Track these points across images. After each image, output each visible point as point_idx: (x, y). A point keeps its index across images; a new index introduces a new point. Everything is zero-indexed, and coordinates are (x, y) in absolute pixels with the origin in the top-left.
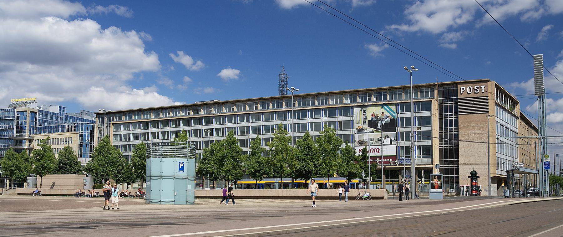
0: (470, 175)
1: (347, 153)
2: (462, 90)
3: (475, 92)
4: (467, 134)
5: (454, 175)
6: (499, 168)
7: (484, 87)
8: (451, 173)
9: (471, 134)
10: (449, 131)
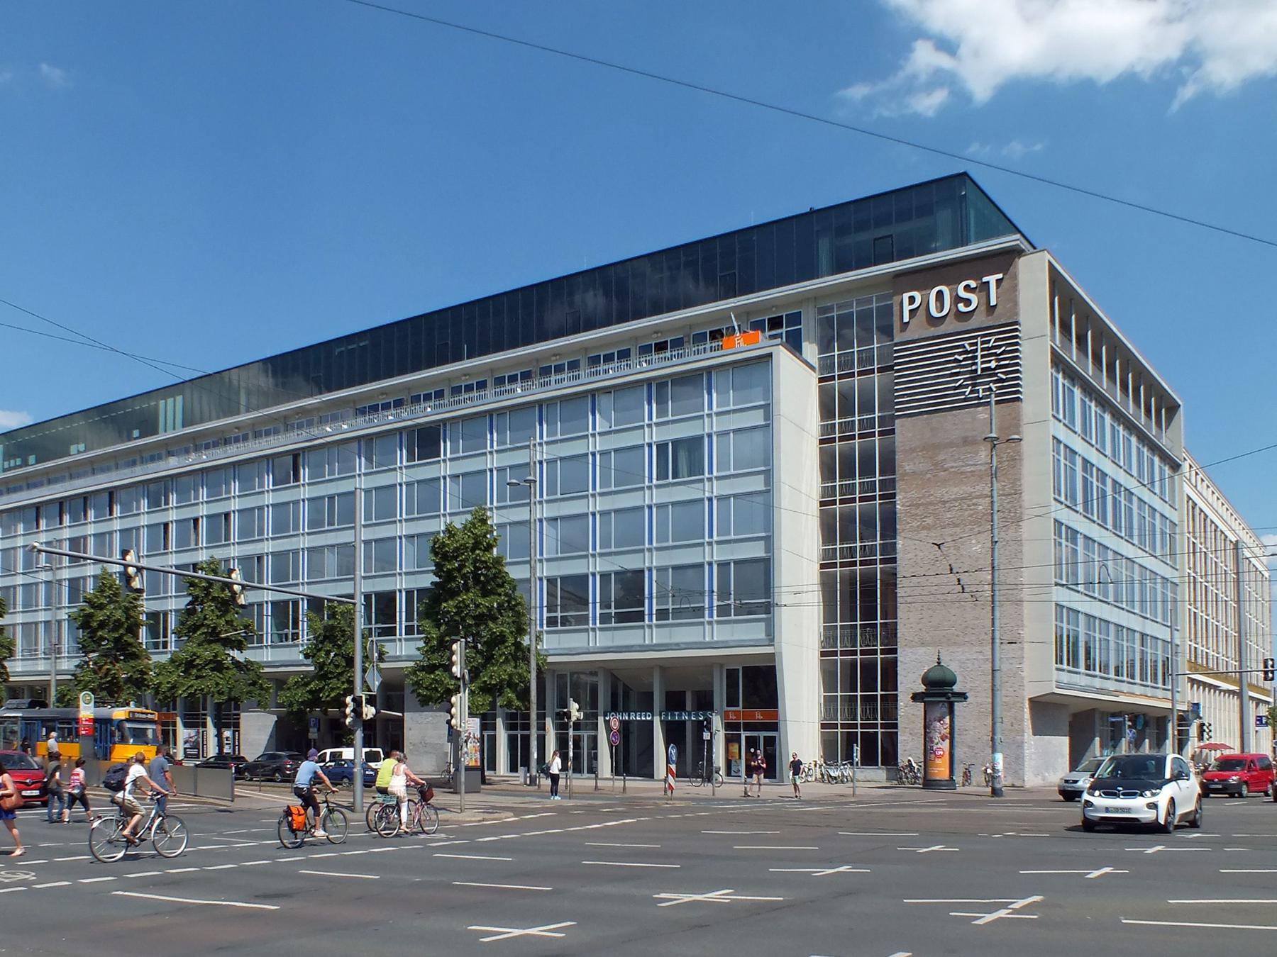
0: (922, 688)
1: (115, 629)
2: (907, 308)
3: (961, 307)
4: (931, 503)
5: (859, 693)
6: (1133, 677)
7: (999, 281)
8: (869, 684)
9: (944, 502)
10: (857, 496)
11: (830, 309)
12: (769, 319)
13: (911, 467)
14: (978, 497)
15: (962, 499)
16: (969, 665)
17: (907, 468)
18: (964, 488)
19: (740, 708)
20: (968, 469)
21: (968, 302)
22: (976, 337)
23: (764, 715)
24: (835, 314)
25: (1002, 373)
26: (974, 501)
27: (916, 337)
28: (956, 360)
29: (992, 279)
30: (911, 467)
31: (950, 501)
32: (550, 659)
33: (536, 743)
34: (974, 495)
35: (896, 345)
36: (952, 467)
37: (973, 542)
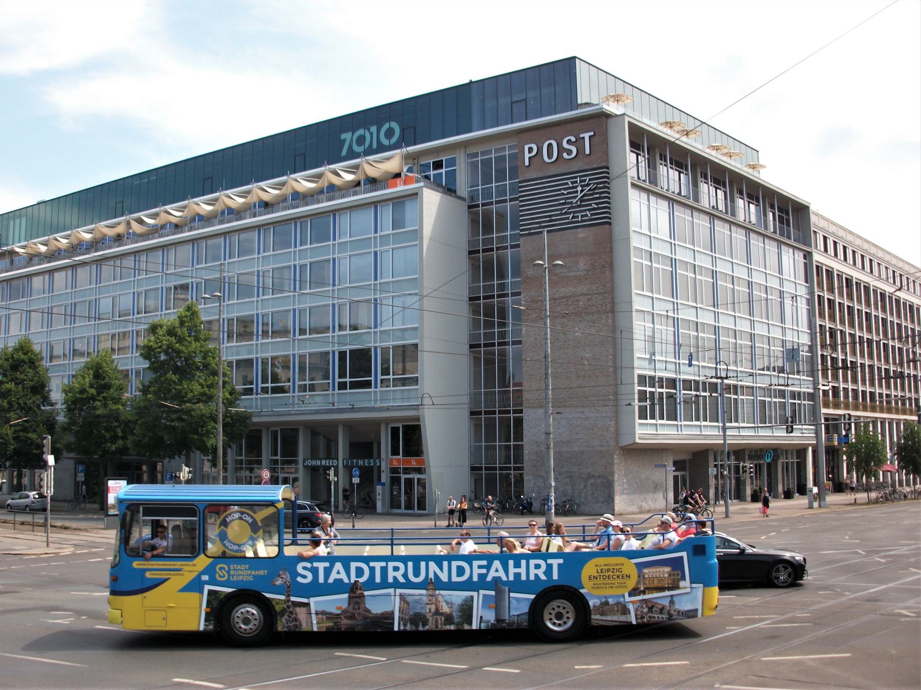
11: (476, 155)
12: (433, 162)
13: (532, 272)
14: (579, 296)
15: (568, 297)
16: (574, 422)
17: (529, 273)
18: (569, 288)
19: (401, 457)
20: (572, 274)
21: (569, 152)
22: (576, 177)
23: (417, 461)
24: (479, 159)
25: (595, 203)
26: (576, 298)
27: (535, 176)
28: (563, 194)
29: (586, 136)
30: (532, 272)
31: (560, 298)
32: (255, 420)
33: (710, 495)
34: (576, 294)
35: (520, 182)
36: (561, 273)
37: (576, 329)
